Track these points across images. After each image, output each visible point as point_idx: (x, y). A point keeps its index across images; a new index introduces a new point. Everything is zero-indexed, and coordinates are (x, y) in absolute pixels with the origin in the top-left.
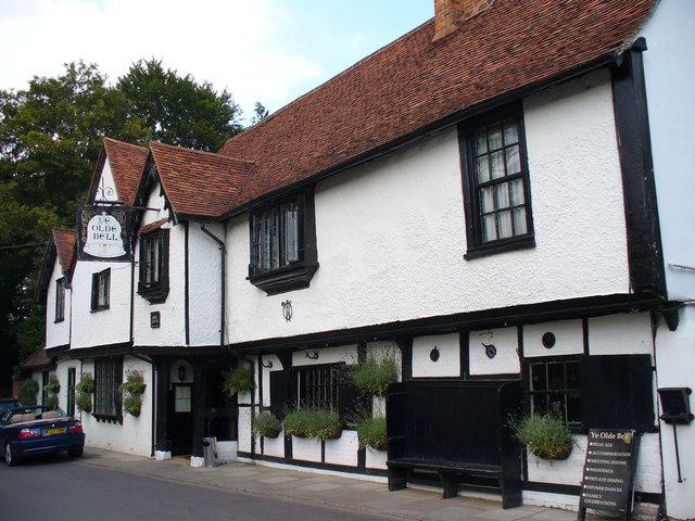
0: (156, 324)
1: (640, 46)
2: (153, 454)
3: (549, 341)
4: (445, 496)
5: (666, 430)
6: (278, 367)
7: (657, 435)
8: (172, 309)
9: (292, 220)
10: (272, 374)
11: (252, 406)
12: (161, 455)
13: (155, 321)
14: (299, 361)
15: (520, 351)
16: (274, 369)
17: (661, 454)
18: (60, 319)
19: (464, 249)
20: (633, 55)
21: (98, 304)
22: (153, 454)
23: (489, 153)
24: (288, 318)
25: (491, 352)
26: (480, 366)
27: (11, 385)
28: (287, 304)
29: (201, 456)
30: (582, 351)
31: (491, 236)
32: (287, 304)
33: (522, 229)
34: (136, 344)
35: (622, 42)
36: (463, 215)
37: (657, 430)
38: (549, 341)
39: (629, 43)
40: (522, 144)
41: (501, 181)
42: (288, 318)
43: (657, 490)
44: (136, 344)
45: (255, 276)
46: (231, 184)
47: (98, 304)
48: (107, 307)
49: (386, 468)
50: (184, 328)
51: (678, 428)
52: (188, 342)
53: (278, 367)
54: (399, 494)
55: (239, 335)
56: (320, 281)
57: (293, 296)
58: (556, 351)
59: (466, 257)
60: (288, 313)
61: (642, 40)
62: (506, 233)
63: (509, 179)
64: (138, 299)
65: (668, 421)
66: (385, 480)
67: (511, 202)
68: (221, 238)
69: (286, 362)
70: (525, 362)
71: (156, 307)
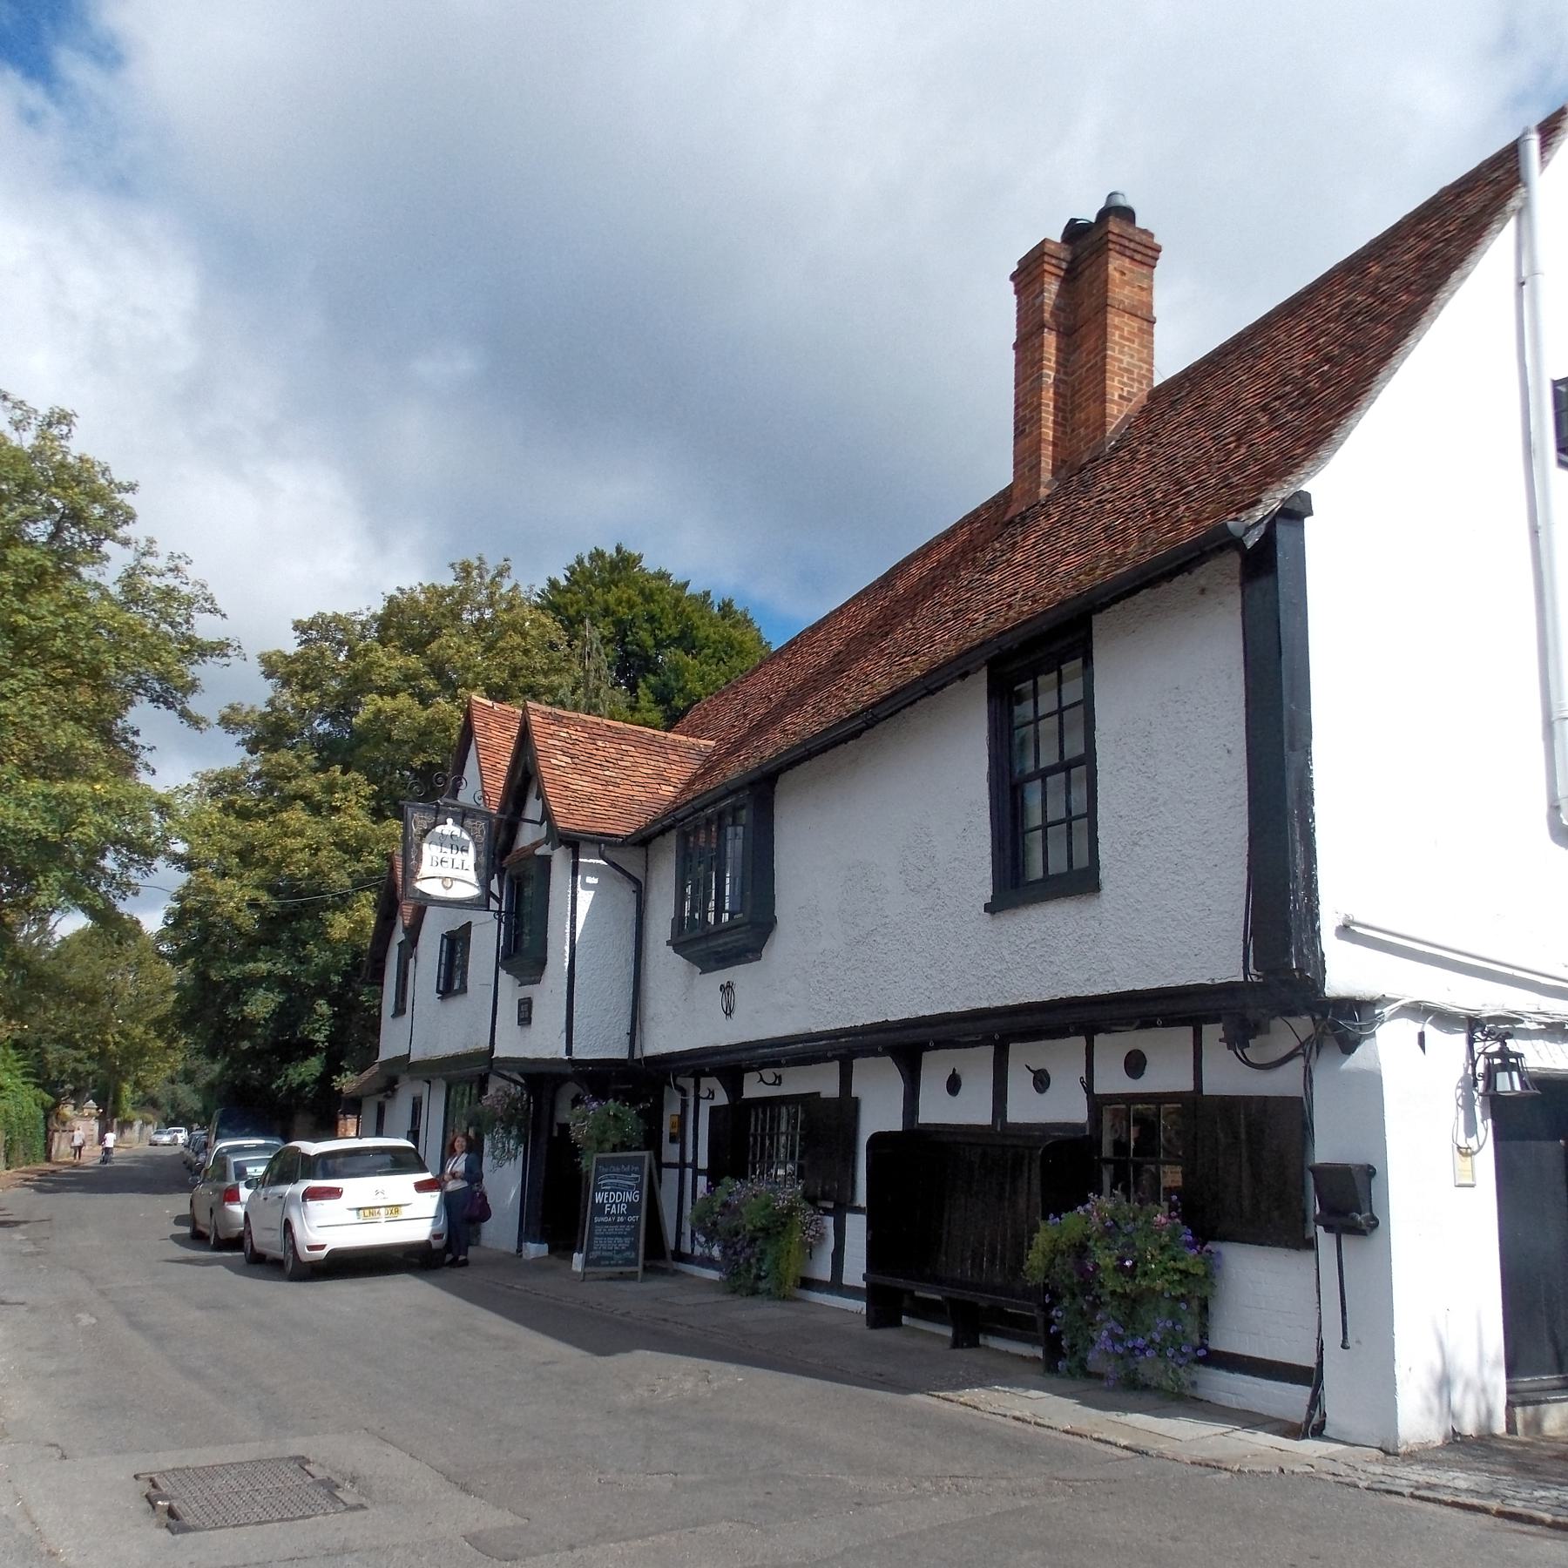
0: (525, 1019)
1: (1296, 511)
2: (519, 1250)
3: (1135, 1064)
4: (956, 1343)
5: (1325, 1240)
6: (722, 1099)
7: (1313, 1254)
8: (549, 994)
9: (735, 844)
10: (713, 1110)
11: (682, 1165)
12: (534, 1250)
13: (525, 1015)
14: (753, 1088)
15: (1088, 1086)
16: (716, 1103)
17: (1319, 1291)
18: (399, 1011)
19: (986, 893)
20: (1282, 530)
21: (451, 982)
22: (519, 1250)
23: (1060, 711)
24: (729, 1012)
25: (1041, 1081)
26: (1026, 1108)
27: (337, 1123)
28: (727, 989)
29: (550, 1251)
30: (1188, 1085)
31: (1036, 871)
32: (727, 989)
33: (1082, 860)
34: (499, 1053)
35: (1260, 501)
36: (988, 832)
37: (1310, 1245)
38: (1135, 1064)
39: (1272, 501)
40: (1088, 703)
41: (1052, 770)
42: (729, 1012)
43: (1311, 1362)
44: (499, 1053)
45: (680, 943)
46: (667, 781)
47: (451, 982)
48: (463, 989)
49: (864, 1285)
50: (563, 1026)
51: (1344, 1237)
52: (569, 1050)
53: (722, 1099)
54: (887, 1335)
55: (663, 1039)
56: (783, 947)
57: (737, 974)
58: (1151, 1083)
59: (989, 908)
60: (728, 1003)
61: (1305, 498)
62: (1058, 864)
63: (1065, 766)
64: (502, 973)
65: (1328, 1229)
66: (860, 1306)
67: (1069, 811)
68: (637, 872)
69: (734, 1087)
70: (1097, 1104)
71: (528, 990)
